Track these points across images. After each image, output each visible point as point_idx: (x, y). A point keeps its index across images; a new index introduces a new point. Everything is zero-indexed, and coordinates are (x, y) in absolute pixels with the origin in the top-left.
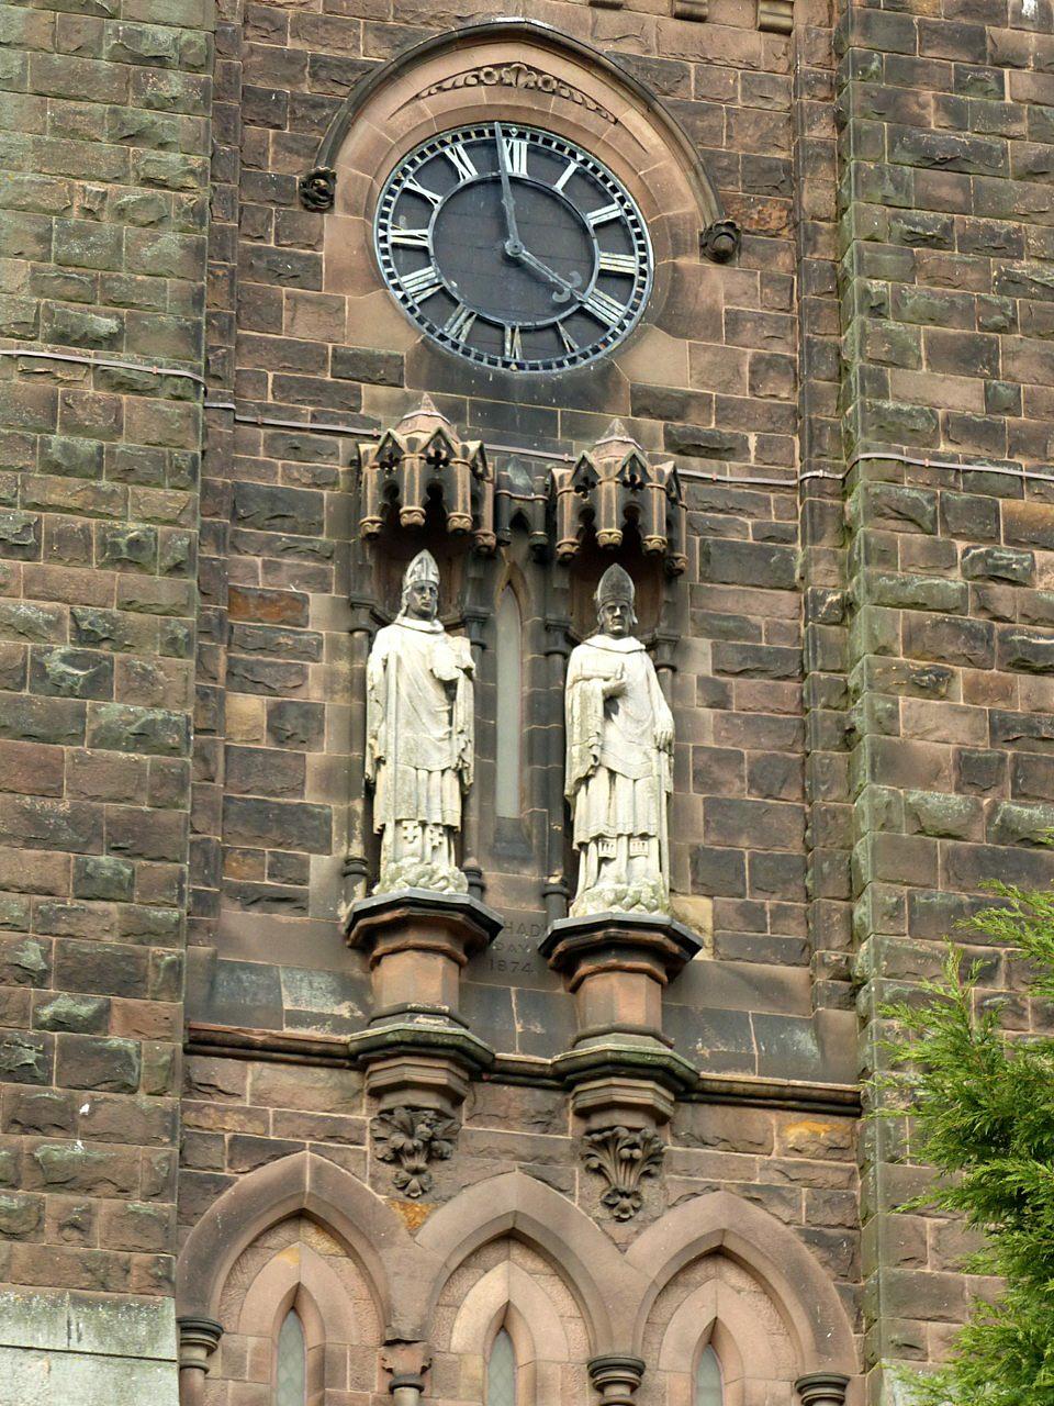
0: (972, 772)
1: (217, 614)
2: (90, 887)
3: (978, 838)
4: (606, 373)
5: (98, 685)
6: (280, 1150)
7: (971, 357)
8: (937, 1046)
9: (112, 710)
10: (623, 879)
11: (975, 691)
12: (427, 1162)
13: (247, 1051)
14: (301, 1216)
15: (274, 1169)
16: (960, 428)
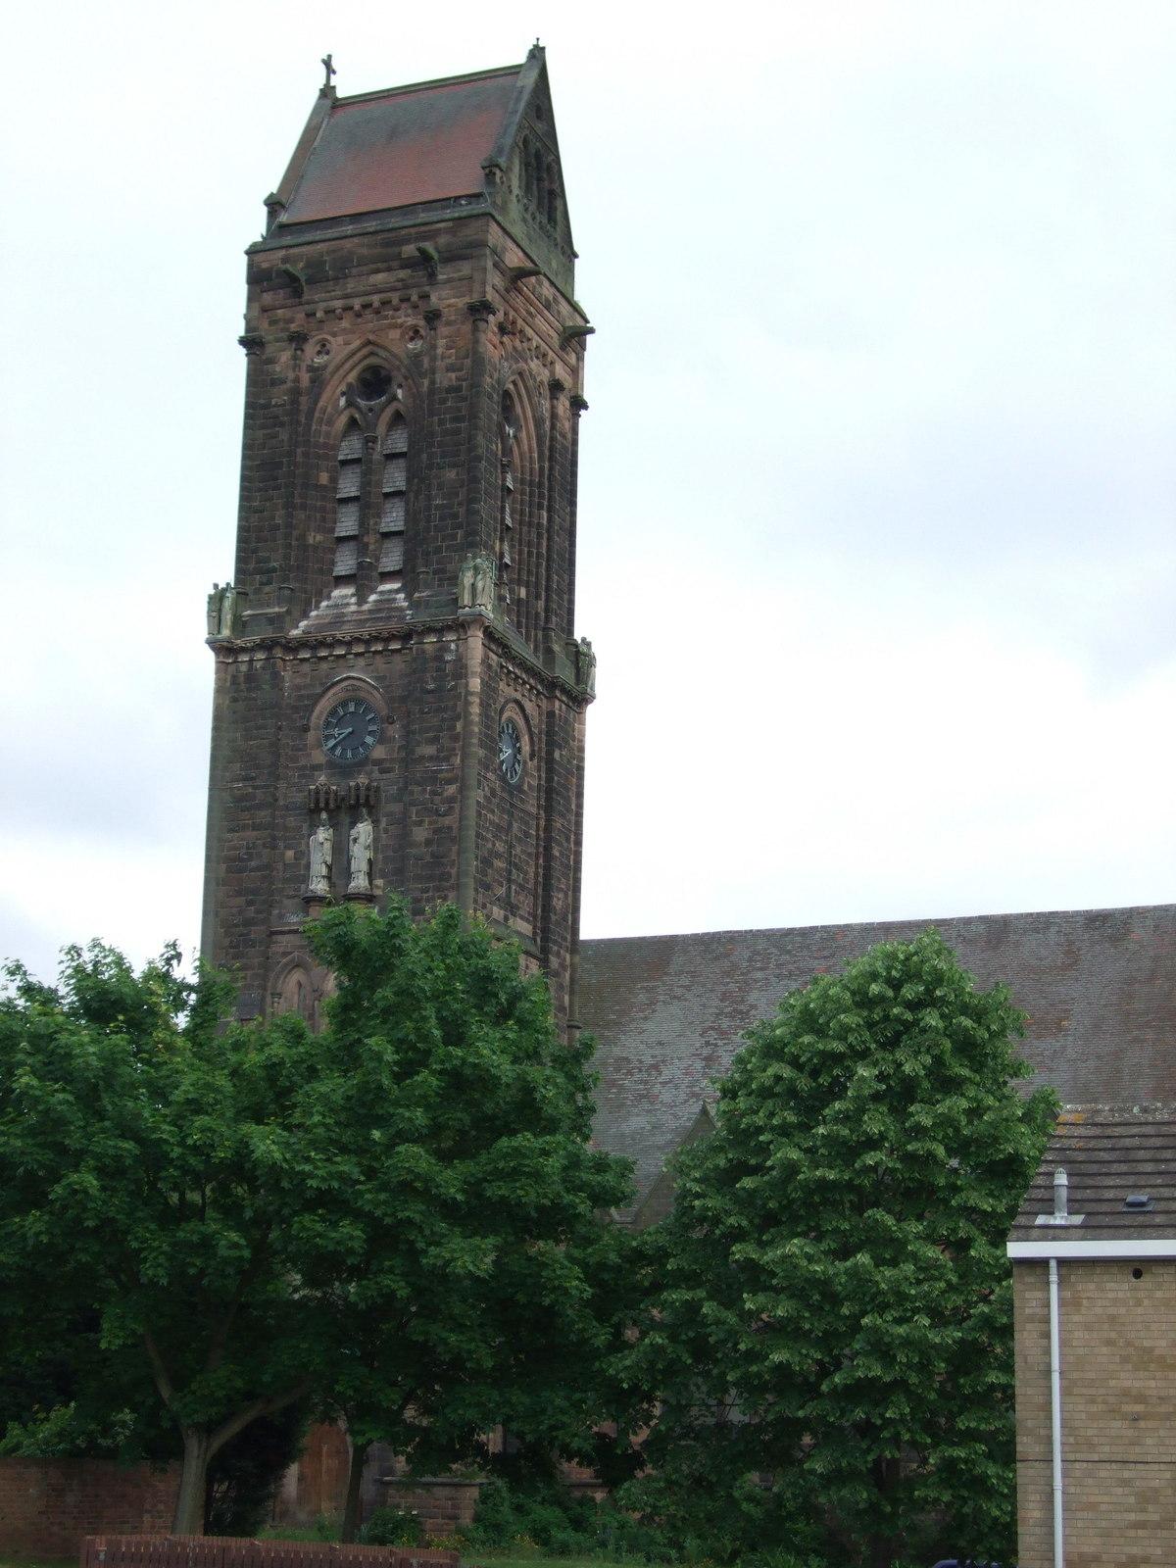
0: (428, 843)
1: (306, 297)
2: (250, 903)
3: (428, 859)
4: (367, 757)
5: (250, 859)
6: (291, 953)
7: (435, 740)
8: (192, 1161)
9: (253, 864)
10: (360, 882)
11: (430, 823)
12: (461, 627)
13: (282, 933)
14: (297, 966)
15: (290, 957)
16: (431, 758)
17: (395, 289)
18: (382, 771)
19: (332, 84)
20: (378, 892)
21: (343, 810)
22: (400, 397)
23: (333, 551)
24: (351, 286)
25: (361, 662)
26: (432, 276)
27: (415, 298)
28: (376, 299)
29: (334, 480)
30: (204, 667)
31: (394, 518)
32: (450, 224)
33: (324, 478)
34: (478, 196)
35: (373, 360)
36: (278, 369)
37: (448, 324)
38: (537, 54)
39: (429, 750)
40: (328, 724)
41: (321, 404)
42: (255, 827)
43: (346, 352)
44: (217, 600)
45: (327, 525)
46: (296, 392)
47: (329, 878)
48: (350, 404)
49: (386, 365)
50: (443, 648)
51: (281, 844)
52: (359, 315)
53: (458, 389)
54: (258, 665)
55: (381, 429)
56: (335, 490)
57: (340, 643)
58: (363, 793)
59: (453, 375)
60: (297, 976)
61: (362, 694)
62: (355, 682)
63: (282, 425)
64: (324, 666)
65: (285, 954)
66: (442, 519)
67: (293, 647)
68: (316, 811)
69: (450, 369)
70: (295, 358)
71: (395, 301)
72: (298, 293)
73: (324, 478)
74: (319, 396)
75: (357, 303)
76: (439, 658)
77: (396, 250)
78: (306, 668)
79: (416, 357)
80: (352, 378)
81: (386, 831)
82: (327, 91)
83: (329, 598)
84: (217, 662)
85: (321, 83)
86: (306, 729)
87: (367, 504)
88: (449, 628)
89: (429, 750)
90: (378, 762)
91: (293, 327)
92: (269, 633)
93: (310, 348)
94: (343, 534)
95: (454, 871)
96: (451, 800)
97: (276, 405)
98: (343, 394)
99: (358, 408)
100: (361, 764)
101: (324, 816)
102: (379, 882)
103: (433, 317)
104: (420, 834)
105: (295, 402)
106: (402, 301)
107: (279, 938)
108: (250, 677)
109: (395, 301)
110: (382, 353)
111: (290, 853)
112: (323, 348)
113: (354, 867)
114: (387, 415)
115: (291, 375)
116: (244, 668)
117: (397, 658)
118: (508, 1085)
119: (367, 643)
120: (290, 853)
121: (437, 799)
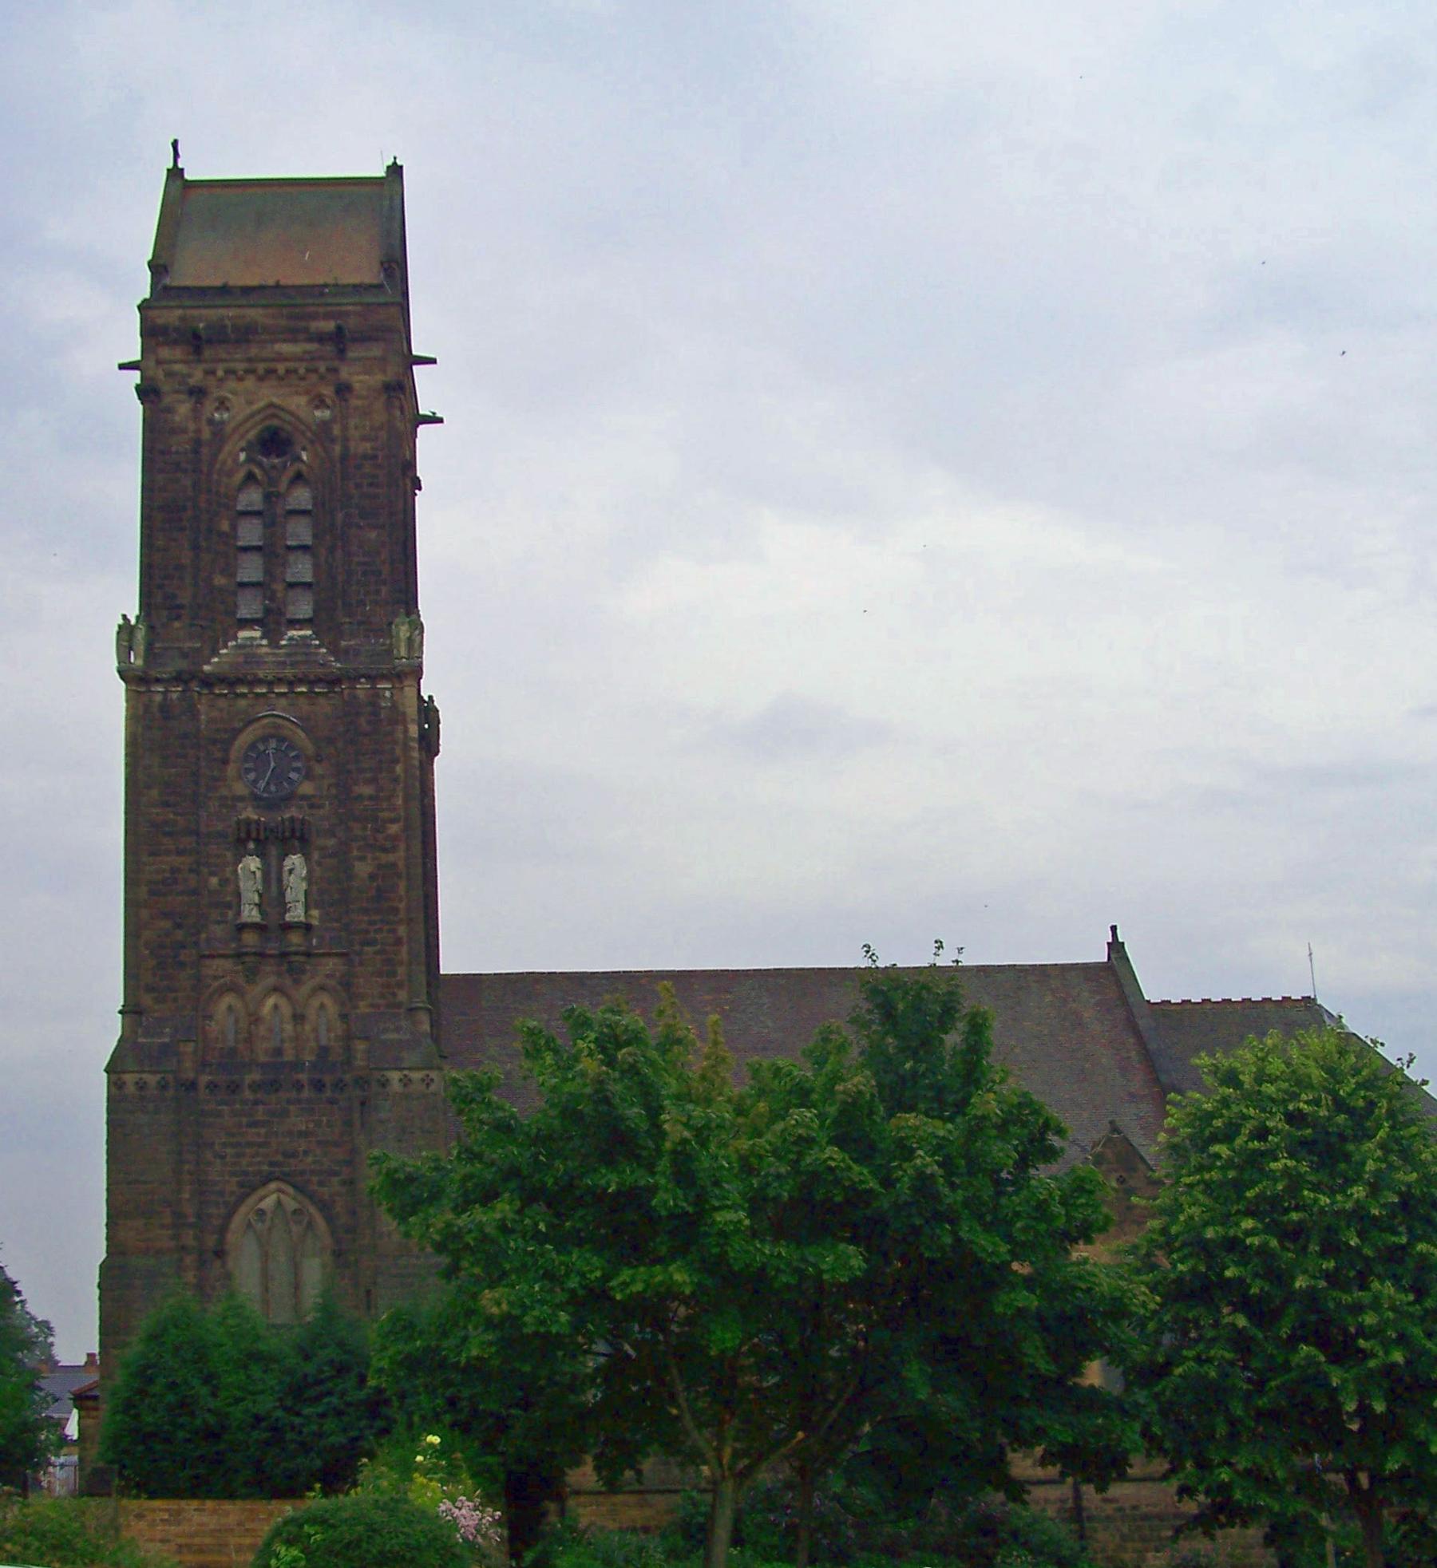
0: (372, 877)
2: (179, 926)
7: (374, 780)
10: (296, 914)
13: (212, 956)
17: (301, 360)
18: (312, 806)
19: (180, 166)
20: (315, 922)
21: (275, 841)
22: (305, 458)
23: (235, 594)
24: (254, 351)
25: (283, 702)
26: (342, 352)
27: (220, 373)
28: (281, 368)
29: (234, 527)
30: (114, 697)
31: (302, 569)
32: (359, 308)
33: (225, 526)
34: (380, 286)
35: (276, 422)
36: (177, 418)
37: (358, 397)
38: (396, 170)
39: (367, 790)
40: (246, 758)
41: (221, 457)
42: (180, 853)
43: (248, 411)
44: (126, 631)
45: (230, 571)
46: (198, 443)
47: (259, 906)
48: (249, 460)
49: (288, 428)
50: (376, 694)
51: (205, 870)
52: (261, 379)
53: (375, 457)
54: (175, 696)
55: (285, 481)
56: (236, 538)
57: (260, 682)
58: (298, 826)
59: (368, 445)
60: (228, 999)
61: (286, 732)
62: (280, 721)
63: (185, 471)
64: (243, 703)
65: (216, 978)
66: (365, 573)
67: (208, 682)
68: (241, 842)
69: (364, 439)
70: (194, 410)
71: (302, 371)
72: (198, 350)
73: (225, 526)
74: (220, 449)
75: (261, 367)
76: (374, 704)
77: (303, 324)
78: (222, 703)
79: (325, 425)
80: (252, 435)
81: (319, 864)
82: (175, 173)
83: (235, 638)
84: (127, 690)
85: (171, 165)
86: (225, 762)
87: (272, 552)
88: (384, 677)
89: (367, 790)
90: (304, 797)
91: (192, 382)
92: (182, 664)
93: (209, 406)
94: (246, 580)
95: (402, 906)
96: (395, 838)
97: (177, 452)
98: (242, 450)
99: (260, 465)
100: (289, 799)
101: (251, 845)
102: (315, 913)
103: (343, 390)
104: (363, 869)
105: (196, 452)
106: (308, 370)
107: (208, 962)
108: (165, 709)
109: (302, 371)
110: (282, 414)
111: (214, 881)
112: (222, 404)
113: (289, 896)
114: (290, 473)
115: (192, 426)
116: (158, 698)
117: (322, 701)
118: (1032, 1263)
119: (270, 684)
120: (214, 881)
121: (380, 836)
